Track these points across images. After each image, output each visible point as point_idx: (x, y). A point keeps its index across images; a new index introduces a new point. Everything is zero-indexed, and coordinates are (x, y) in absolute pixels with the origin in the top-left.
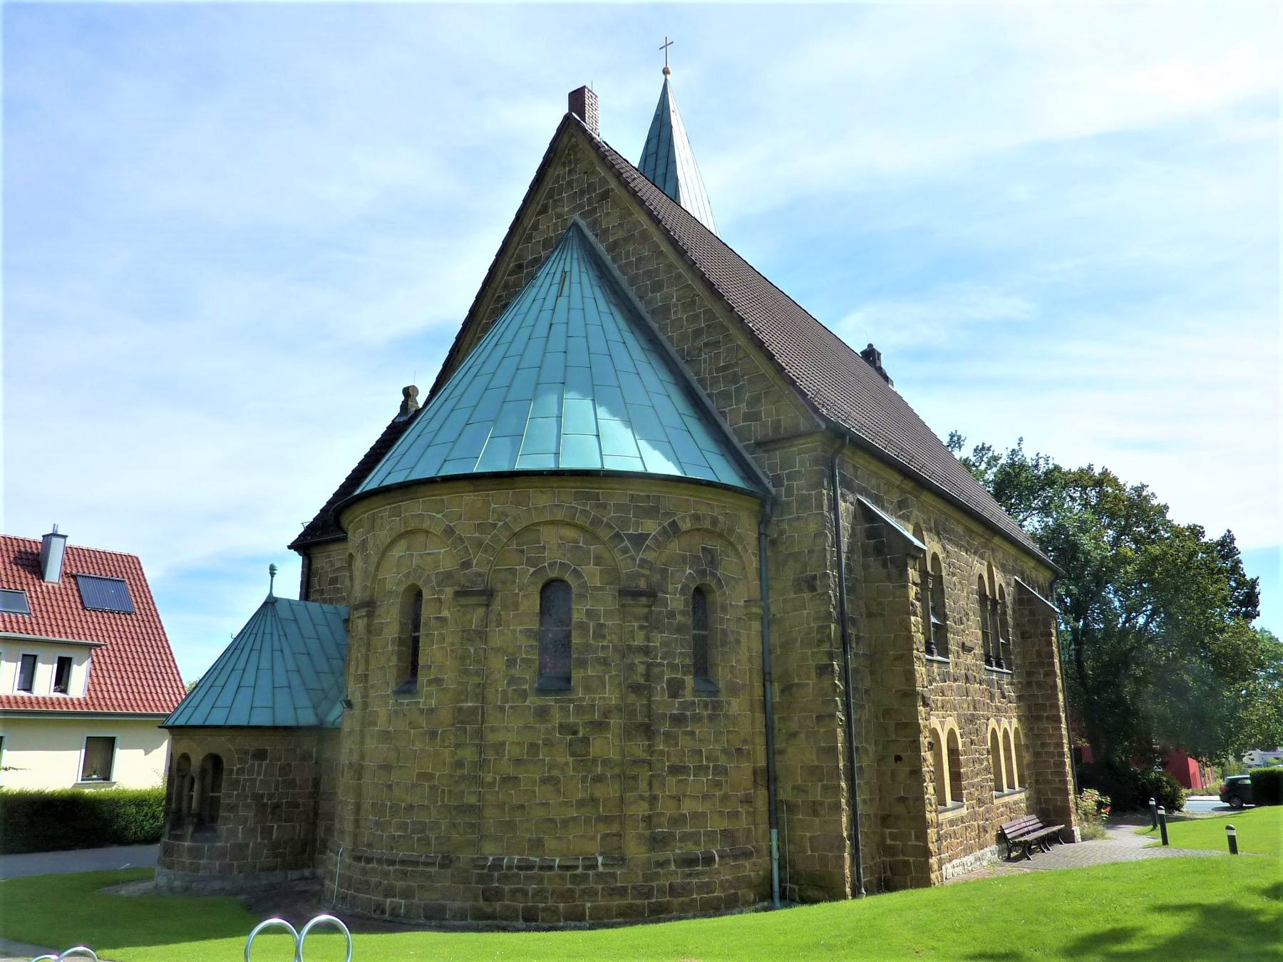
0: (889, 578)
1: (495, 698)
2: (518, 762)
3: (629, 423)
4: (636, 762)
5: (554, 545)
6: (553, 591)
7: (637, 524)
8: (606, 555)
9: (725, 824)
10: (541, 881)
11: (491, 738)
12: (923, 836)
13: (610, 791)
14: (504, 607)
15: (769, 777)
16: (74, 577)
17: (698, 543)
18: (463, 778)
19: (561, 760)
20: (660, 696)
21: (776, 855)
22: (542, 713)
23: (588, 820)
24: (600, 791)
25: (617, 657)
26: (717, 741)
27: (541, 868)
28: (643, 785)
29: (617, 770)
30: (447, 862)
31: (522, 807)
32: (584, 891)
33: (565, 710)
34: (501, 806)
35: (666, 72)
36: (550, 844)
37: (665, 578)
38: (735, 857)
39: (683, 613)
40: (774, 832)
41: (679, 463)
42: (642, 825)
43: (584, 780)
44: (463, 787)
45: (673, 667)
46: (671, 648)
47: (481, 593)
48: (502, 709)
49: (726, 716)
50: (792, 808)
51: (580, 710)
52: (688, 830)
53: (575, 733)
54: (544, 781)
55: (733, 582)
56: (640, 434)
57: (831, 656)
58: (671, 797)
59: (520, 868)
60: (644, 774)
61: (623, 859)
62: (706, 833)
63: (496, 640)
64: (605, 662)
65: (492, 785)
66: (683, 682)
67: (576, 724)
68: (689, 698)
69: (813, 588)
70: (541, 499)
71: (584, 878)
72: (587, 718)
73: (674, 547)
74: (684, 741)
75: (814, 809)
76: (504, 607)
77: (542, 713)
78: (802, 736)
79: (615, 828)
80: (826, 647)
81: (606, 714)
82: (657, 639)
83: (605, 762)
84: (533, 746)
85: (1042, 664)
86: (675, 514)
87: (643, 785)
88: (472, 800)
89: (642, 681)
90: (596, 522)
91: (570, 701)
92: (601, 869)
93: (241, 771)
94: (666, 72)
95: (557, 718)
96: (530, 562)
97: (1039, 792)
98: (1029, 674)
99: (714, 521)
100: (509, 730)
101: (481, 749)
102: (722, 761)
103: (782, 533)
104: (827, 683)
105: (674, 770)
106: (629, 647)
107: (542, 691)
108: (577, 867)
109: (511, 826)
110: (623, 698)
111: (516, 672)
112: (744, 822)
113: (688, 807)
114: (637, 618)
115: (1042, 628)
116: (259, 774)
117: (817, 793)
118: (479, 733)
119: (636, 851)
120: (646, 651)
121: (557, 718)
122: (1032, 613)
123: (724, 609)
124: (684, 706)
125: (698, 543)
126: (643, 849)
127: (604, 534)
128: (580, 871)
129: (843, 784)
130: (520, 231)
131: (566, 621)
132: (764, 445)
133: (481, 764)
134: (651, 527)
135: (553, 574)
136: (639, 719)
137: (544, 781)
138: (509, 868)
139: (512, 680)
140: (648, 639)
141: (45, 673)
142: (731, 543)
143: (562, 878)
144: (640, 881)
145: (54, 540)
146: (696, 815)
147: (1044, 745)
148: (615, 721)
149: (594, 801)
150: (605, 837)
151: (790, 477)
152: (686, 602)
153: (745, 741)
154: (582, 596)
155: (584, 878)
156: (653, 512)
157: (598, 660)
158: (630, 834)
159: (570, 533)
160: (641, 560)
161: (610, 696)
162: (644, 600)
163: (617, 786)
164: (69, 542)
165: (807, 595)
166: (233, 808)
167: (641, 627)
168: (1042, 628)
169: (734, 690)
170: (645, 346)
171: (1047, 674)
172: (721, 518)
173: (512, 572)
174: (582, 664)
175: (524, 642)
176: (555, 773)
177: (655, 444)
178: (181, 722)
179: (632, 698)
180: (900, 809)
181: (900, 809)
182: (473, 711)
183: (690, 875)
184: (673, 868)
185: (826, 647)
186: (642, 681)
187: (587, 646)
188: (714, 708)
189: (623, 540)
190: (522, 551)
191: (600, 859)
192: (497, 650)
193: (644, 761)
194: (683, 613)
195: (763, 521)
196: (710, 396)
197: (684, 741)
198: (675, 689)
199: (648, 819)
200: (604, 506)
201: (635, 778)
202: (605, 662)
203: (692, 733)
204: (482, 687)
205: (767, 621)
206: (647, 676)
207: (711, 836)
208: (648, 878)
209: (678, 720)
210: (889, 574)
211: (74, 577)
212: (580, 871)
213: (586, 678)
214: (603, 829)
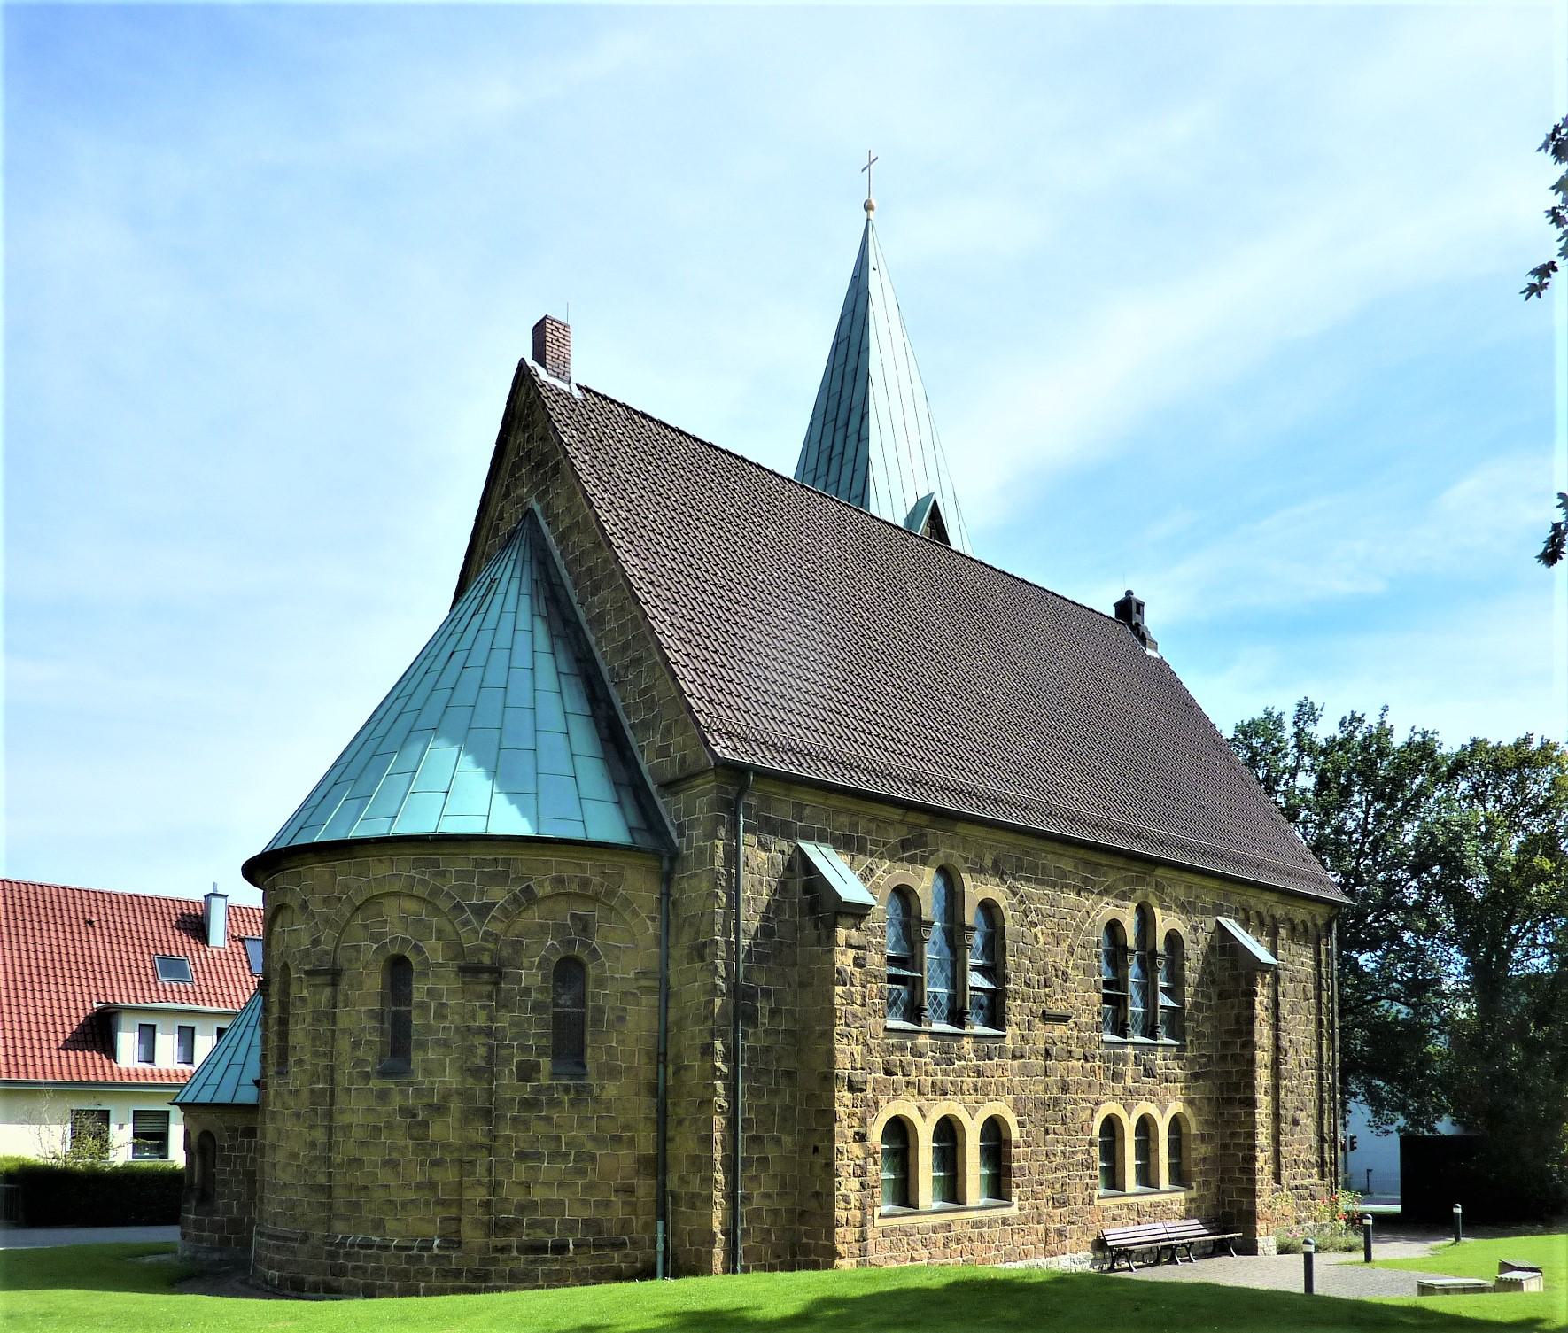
0: (819, 941)
1: (341, 1079)
2: (362, 1143)
3: (493, 773)
4: (476, 1147)
5: (395, 919)
6: (399, 970)
7: (482, 892)
8: (448, 928)
9: (588, 1213)
10: (378, 1259)
11: (342, 1119)
12: (831, 1235)
13: (449, 1175)
14: (351, 986)
15: (657, 1165)
16: (242, 940)
17: (565, 911)
18: (316, 1158)
19: (401, 1143)
20: (507, 1081)
21: (660, 1247)
22: (383, 1095)
23: (427, 1203)
24: (438, 1175)
25: (457, 1038)
26: (581, 1126)
27: (380, 1247)
28: (481, 1171)
29: (456, 1155)
30: (305, 1238)
31: (366, 1188)
32: (417, 1271)
33: (404, 1093)
34: (349, 1187)
35: (868, 207)
36: (391, 1224)
37: (517, 952)
38: (598, 1247)
39: (539, 990)
40: (660, 1224)
41: (538, 820)
42: (479, 1210)
43: (422, 1164)
44: (315, 1167)
45: (525, 1049)
46: (522, 1030)
47: (325, 972)
48: (349, 1090)
49: (596, 1101)
50: (676, 1198)
51: (419, 1093)
52: (539, 1216)
53: (414, 1116)
54: (386, 1163)
55: (616, 952)
56: (500, 787)
57: (713, 1035)
58: (520, 1184)
59: (361, 1246)
60: (483, 1159)
61: (459, 1243)
62: (563, 1222)
63: (344, 1021)
64: (446, 1044)
65: (340, 1165)
66: (538, 1064)
67: (415, 1108)
68: (545, 1081)
69: (702, 958)
70: (380, 869)
71: (419, 1259)
72: (426, 1101)
73: (533, 916)
74: (536, 1128)
75: (693, 1200)
76: (351, 986)
77: (383, 1095)
78: (687, 1123)
79: (453, 1212)
80: (709, 1025)
81: (446, 1097)
82: (505, 1020)
83: (445, 1146)
84: (376, 1129)
85: (1238, 1033)
86: (530, 879)
87: (481, 1171)
88: (322, 1180)
89: (483, 1064)
90: (436, 892)
91: (411, 1084)
92: (436, 1251)
93: (231, 1148)
94: (868, 207)
95: (397, 1101)
96: (374, 939)
97: (1220, 1191)
98: (1225, 1044)
99: (585, 883)
100: (355, 1112)
101: (330, 1130)
102: (589, 1147)
103: (682, 892)
104: (708, 1065)
105: (523, 1156)
106: (469, 1029)
107: (384, 1074)
108: (411, 1248)
109: (356, 1206)
110: (463, 1081)
111: (360, 1054)
112: (619, 1211)
113: (538, 1194)
114: (479, 997)
115: (1244, 986)
116: (249, 1150)
117: (695, 1185)
118: (329, 1115)
119: (472, 1236)
120: (489, 1032)
121: (397, 1101)
122: (1234, 966)
123: (600, 982)
124: (538, 1090)
125: (565, 911)
126: (480, 1233)
127: (445, 905)
128: (415, 1251)
129: (719, 1176)
130: (487, 523)
131: (407, 999)
132: (670, 786)
133: (330, 1146)
134: (499, 895)
135: (395, 950)
136: (478, 1104)
137: (386, 1163)
138: (352, 1246)
139: (358, 1063)
140: (491, 1019)
141: (167, 1044)
142: (612, 908)
143: (398, 1257)
144: (476, 1265)
145: (214, 900)
146: (547, 1203)
147: (1233, 1135)
148: (455, 1105)
149: (432, 1185)
150: (443, 1220)
151: (691, 828)
152: (545, 979)
153: (627, 1127)
154: (424, 974)
155: (419, 1259)
156: (501, 878)
157: (438, 1042)
158: (466, 1219)
159: (410, 905)
160: (486, 932)
161: (451, 1079)
162: (485, 977)
163: (456, 1171)
164: (230, 901)
165: (698, 965)
166: (226, 1183)
167: (483, 1007)
168: (1244, 986)
169: (612, 1073)
170: (564, 668)
171: (1244, 1046)
172: (596, 880)
173: (357, 949)
174: (422, 1045)
175: (369, 1023)
176: (395, 1155)
177: (513, 796)
178: (205, 1097)
179: (470, 1081)
180: (812, 1205)
181: (812, 1205)
182: (323, 1091)
183: (532, 1262)
184: (515, 1254)
185: (709, 1025)
186: (483, 1064)
187: (428, 1027)
188: (578, 1092)
189: (463, 910)
190: (366, 926)
191: (437, 1242)
192: (344, 1031)
193: (482, 1146)
194: (539, 990)
195: (667, 879)
196: (632, 726)
197: (536, 1128)
198: (527, 1072)
199: (487, 1205)
200: (443, 874)
201: (472, 1163)
202: (446, 1044)
203: (548, 1119)
204: (332, 1069)
205: (665, 993)
206: (488, 1059)
207: (570, 1226)
208: (483, 1262)
209: (527, 1105)
210: (819, 937)
211: (242, 940)
212: (415, 1251)
213: (426, 1060)
214: (441, 1213)
